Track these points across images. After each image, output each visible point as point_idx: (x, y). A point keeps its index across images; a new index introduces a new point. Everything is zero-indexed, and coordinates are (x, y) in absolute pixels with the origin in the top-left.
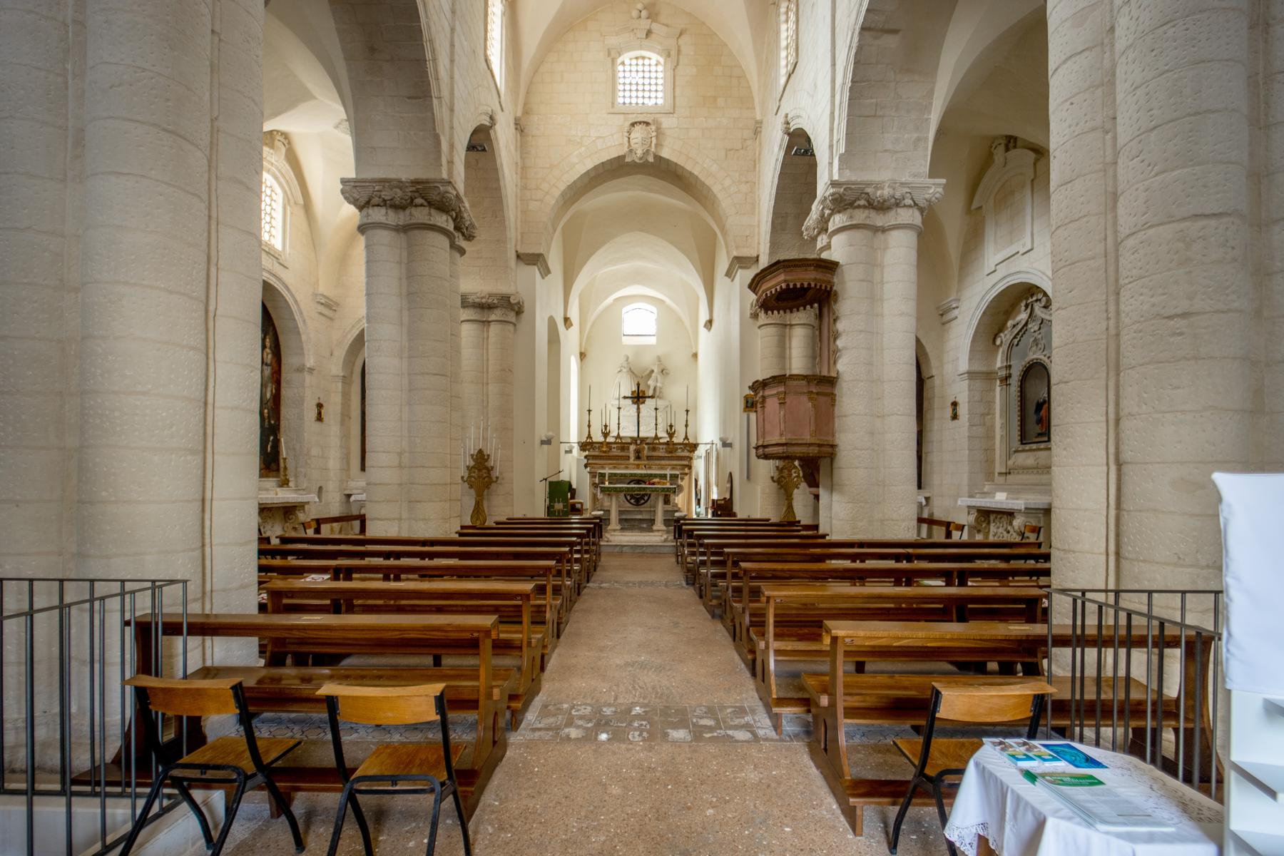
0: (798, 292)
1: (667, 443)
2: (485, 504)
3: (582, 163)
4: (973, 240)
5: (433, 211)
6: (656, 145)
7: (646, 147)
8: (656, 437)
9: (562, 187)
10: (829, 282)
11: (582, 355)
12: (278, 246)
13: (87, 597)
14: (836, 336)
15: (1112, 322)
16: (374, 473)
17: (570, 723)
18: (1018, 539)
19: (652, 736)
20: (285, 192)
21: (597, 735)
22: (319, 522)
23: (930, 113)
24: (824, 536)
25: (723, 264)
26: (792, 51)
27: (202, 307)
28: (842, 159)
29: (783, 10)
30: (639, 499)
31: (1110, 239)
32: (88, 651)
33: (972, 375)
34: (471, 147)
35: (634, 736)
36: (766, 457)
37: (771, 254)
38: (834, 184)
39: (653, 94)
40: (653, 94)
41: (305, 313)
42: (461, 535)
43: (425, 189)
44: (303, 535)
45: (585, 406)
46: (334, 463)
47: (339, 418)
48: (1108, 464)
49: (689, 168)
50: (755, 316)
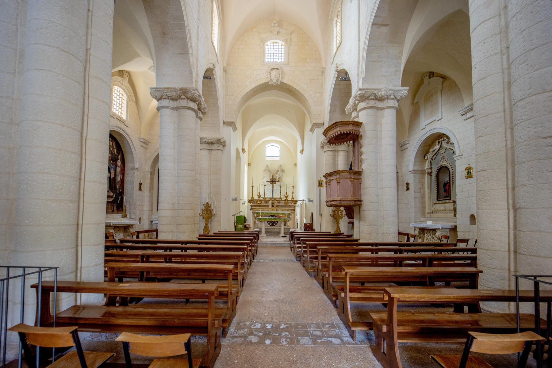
0: (346, 136)
1: (285, 200)
2: (209, 225)
3: (250, 86)
4: (415, 115)
5: (189, 101)
7: (277, 79)
8: (280, 198)
9: (242, 95)
10: (358, 131)
11: (249, 164)
12: (124, 117)
13: (6, 277)
14: (361, 154)
15: (509, 143)
16: (162, 212)
17: (251, 334)
19: (292, 342)
20: (128, 96)
21: (265, 340)
22: (138, 233)
23: (401, 60)
24: (357, 240)
25: (308, 126)
26: (340, 39)
27: (79, 133)
28: (363, 79)
29: (334, 22)
30: (273, 224)
31: (507, 104)
33: (415, 172)
34: (205, 77)
35: (283, 341)
36: (331, 206)
37: (329, 121)
38: (360, 90)
39: (280, 57)
40: (280, 57)
41: (135, 145)
42: (199, 239)
44: (132, 239)
45: (249, 185)
46: (146, 208)
47: (148, 189)
48: (508, 209)
49: (295, 87)
50: (323, 147)
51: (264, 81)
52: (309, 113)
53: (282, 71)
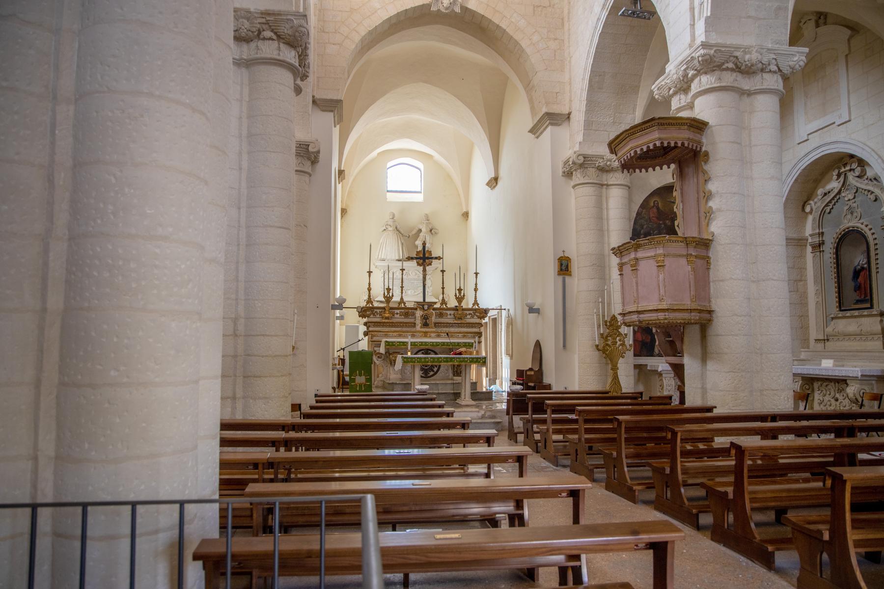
1: (456, 309)
5: (282, 45)
14: (709, 196)
18: (855, 408)
32: (78, 577)
43: (276, 21)
49: (496, 21)
50: (568, 174)
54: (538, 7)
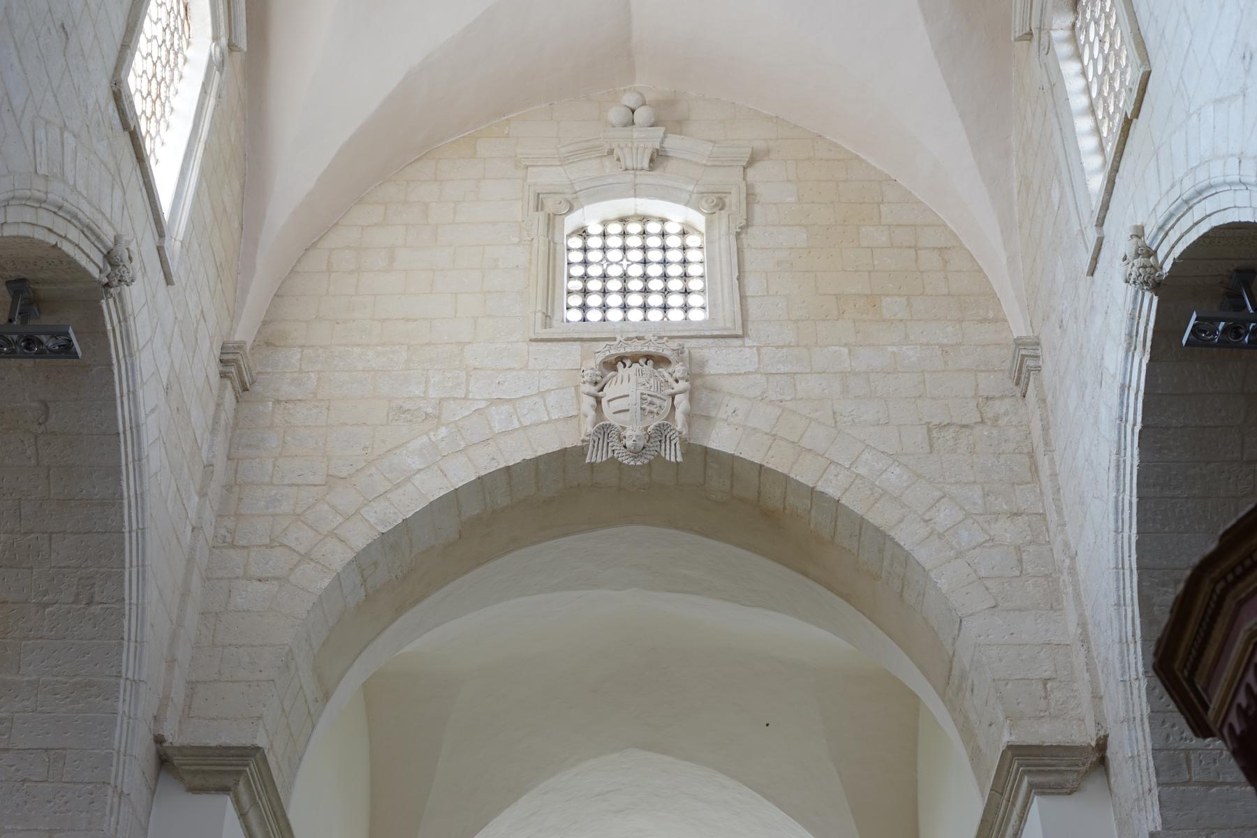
3: (432, 467)
6: (690, 417)
9: (360, 538)
49: (804, 474)
51: (548, 444)
52: (950, 681)
53: (691, 377)
54: (941, 427)
